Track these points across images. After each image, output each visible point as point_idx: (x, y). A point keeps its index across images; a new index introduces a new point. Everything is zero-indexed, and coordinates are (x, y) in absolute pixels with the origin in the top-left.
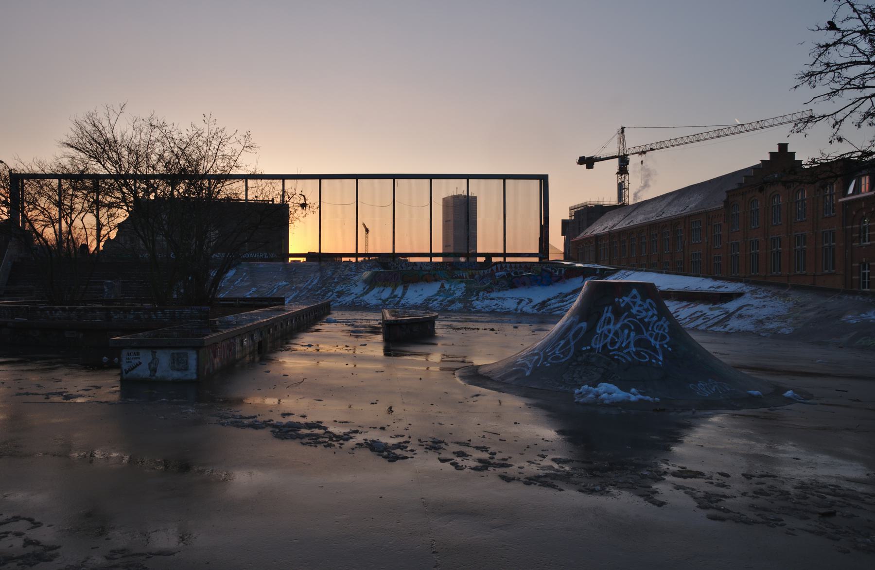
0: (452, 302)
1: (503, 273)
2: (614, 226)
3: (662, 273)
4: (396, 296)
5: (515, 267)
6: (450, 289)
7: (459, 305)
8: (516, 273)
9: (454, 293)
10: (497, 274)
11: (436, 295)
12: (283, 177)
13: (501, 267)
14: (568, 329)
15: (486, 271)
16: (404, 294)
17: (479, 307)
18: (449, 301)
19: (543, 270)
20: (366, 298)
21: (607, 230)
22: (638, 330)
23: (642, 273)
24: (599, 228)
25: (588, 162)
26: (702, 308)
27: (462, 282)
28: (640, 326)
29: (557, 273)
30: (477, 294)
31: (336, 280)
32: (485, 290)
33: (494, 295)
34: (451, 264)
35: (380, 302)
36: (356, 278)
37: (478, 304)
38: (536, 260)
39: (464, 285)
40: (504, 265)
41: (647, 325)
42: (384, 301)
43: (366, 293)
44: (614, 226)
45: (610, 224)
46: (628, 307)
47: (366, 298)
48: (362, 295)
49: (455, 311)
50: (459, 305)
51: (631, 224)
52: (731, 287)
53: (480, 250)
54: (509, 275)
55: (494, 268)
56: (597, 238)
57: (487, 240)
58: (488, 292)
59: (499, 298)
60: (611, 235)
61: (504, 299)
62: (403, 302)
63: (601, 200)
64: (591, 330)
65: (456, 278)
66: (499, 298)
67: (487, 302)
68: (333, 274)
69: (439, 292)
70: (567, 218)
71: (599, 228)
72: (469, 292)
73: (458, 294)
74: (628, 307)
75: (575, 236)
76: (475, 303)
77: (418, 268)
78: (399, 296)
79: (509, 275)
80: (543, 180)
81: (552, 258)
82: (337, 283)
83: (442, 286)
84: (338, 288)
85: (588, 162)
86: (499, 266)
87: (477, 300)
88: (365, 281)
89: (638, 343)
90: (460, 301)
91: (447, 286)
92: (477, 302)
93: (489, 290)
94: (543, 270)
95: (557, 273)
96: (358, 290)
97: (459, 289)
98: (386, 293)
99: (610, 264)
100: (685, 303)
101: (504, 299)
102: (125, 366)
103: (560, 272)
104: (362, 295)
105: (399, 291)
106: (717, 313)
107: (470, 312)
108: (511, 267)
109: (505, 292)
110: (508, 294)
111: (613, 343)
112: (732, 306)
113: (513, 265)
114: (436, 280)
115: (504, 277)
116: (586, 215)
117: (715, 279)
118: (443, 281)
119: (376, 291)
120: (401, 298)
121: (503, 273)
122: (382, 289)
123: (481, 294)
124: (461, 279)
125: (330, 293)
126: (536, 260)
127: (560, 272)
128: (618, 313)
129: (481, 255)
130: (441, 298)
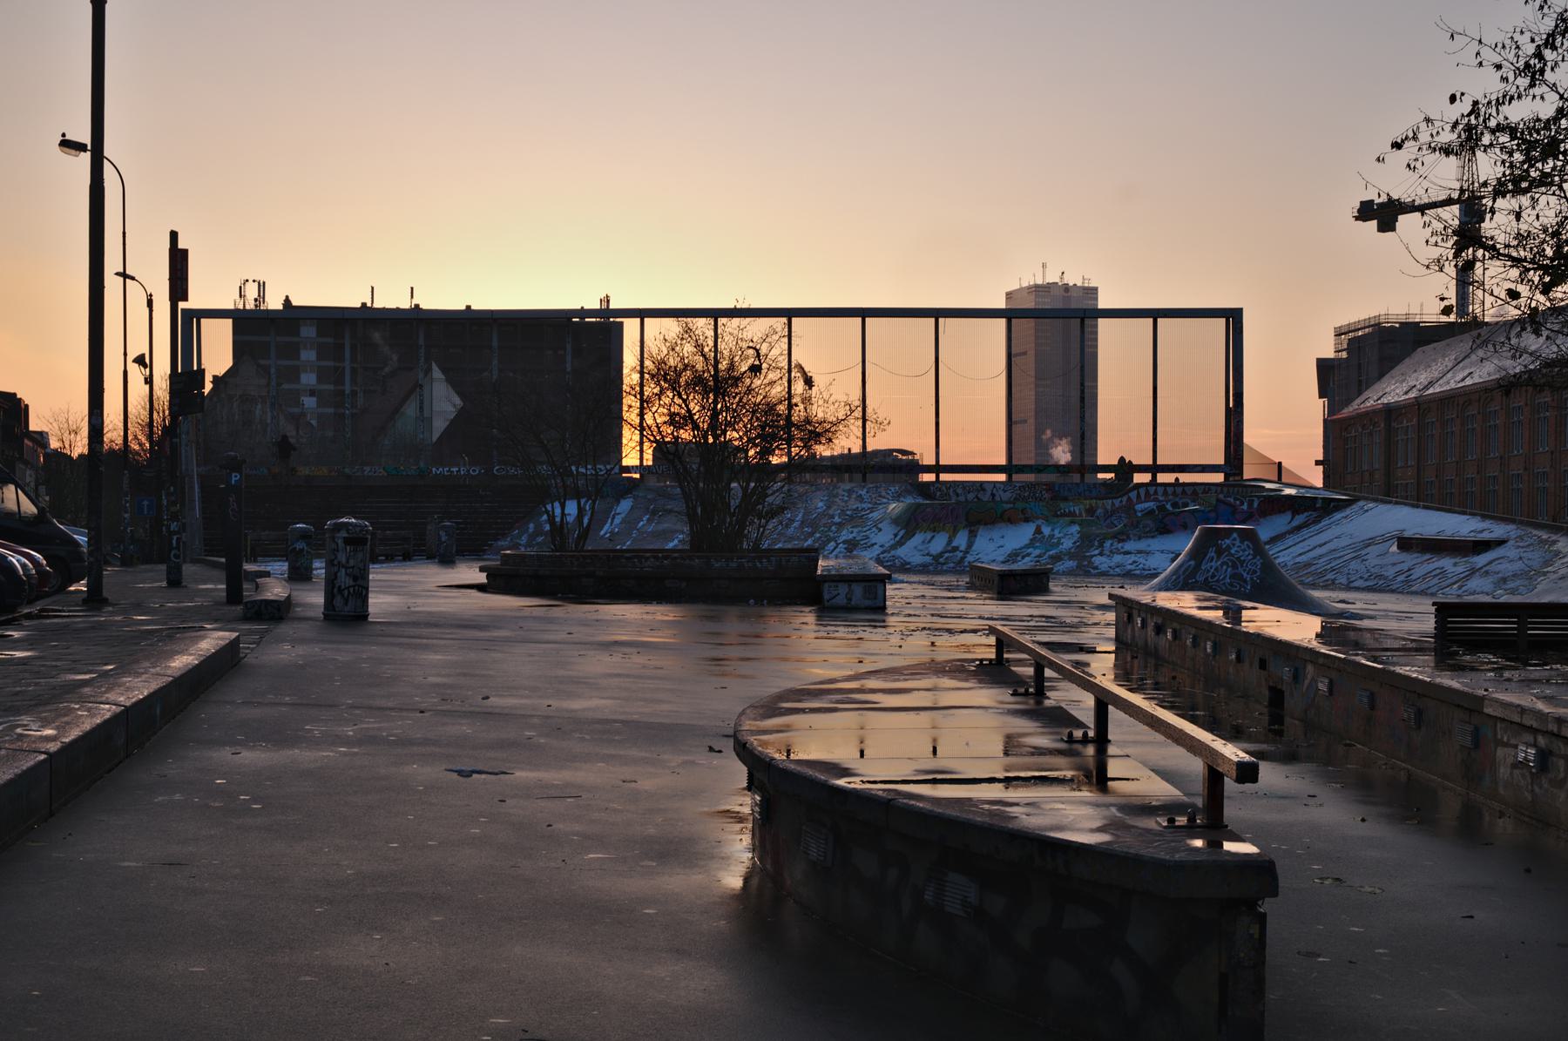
0: (1057, 558)
1: (1151, 505)
2: (1431, 384)
3: (1417, 507)
4: (956, 549)
5: (1174, 493)
6: (1052, 536)
7: (1071, 564)
8: (1175, 505)
9: (1059, 544)
10: (1139, 507)
11: (1027, 546)
12: (715, 314)
13: (1147, 492)
14: (1180, 566)
15: (1117, 502)
16: (970, 545)
17: (1104, 567)
18: (1051, 557)
19: (1218, 500)
20: (903, 552)
21: (1412, 395)
22: (1234, 566)
23: (1389, 506)
24: (1394, 390)
25: (1384, 214)
26: (1447, 563)
27: (1073, 522)
28: (1236, 563)
29: (1245, 507)
30: (1101, 545)
31: (837, 519)
32: (1114, 537)
33: (1130, 546)
34: (1050, 487)
35: (928, 559)
36: (875, 515)
37: (1101, 562)
38: (1218, 478)
39: (1075, 528)
40: (1152, 490)
41: (1242, 563)
42: (936, 558)
43: (901, 543)
44: (1431, 384)
45: (1423, 377)
46: (1229, 548)
47: (903, 552)
48: (893, 547)
49: (1064, 573)
50: (1071, 564)
51: (1468, 382)
52: (1497, 530)
53: (1102, 460)
54: (1161, 508)
55: (1133, 495)
56: (1390, 412)
57: (1118, 437)
58: (1120, 541)
59: (1140, 552)
60: (1421, 406)
61: (1148, 553)
62: (970, 558)
63: (1415, 310)
64: (1198, 566)
65: (1063, 515)
66: (1140, 552)
67: (1118, 558)
68: (829, 507)
69: (1033, 541)
70: (1329, 354)
71: (1394, 390)
72: (1086, 541)
73: (1067, 544)
74: (1229, 548)
75: (1349, 402)
76: (1097, 560)
77: (986, 497)
78: (963, 548)
79: (1161, 508)
80: (1233, 318)
81: (1248, 473)
82: (839, 524)
83: (1038, 531)
84: (845, 535)
85: (1384, 214)
86: (1142, 491)
87: (1101, 554)
88: (896, 521)
89: (1233, 576)
90: (1071, 556)
91: (1046, 530)
92: (1103, 559)
93: (1122, 537)
94: (1218, 500)
95: (1245, 507)
96: (885, 536)
97: (1068, 537)
98: (939, 544)
99: (1344, 491)
100: (1427, 556)
101: (1148, 553)
102: (826, 596)
103: (1251, 503)
104: (893, 547)
105: (961, 540)
106: (1460, 569)
107: (1087, 574)
108: (1165, 493)
109: (1150, 541)
110: (1156, 544)
111: (1213, 576)
112: (1481, 560)
113: (1170, 490)
114: (1027, 520)
115: (1150, 513)
116: (1373, 349)
117: (1484, 517)
118: (1039, 522)
119: (918, 539)
120: (966, 552)
121: (1151, 505)
122: (929, 535)
123: (1108, 544)
124: (1072, 517)
125: (832, 544)
126: (1218, 478)
127: (1251, 503)
128: (1220, 552)
129: (1106, 468)
130: (1037, 552)
